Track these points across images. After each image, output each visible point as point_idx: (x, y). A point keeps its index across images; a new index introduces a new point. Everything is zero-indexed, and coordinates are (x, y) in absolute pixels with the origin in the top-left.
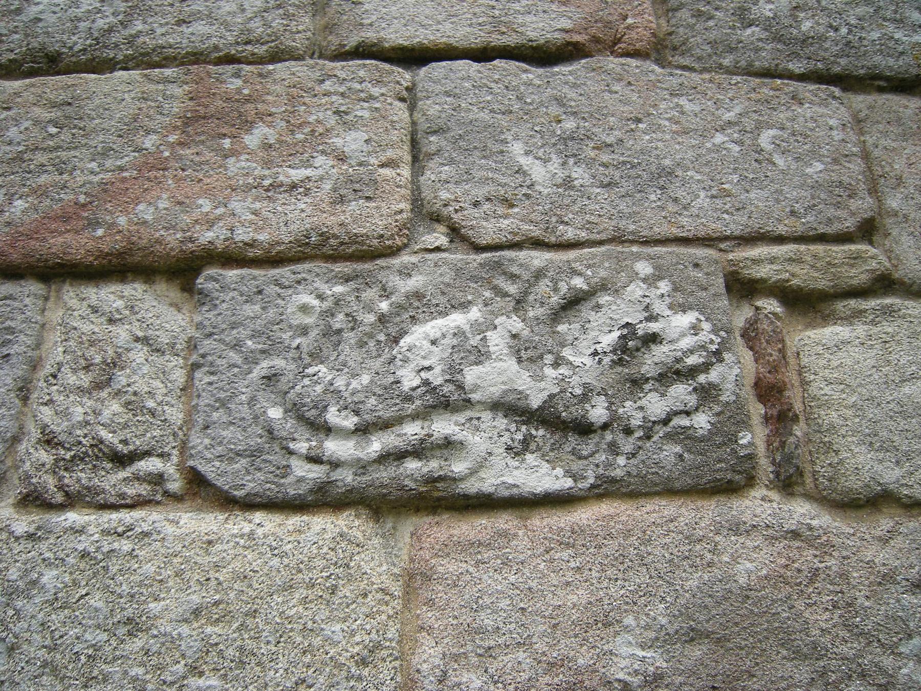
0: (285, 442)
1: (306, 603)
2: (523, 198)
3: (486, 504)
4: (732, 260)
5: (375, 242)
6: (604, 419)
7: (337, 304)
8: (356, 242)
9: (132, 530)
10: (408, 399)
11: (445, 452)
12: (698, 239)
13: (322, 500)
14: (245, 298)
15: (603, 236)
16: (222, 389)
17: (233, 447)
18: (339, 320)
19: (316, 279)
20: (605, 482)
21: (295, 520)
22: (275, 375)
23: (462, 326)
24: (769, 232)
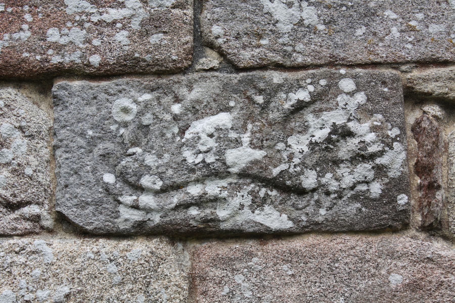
0: (116, 197)
1: (132, 292)
2: (270, 33)
3: (237, 235)
4: (409, 79)
5: (170, 65)
6: (313, 186)
7: (146, 107)
8: (158, 65)
9: (24, 249)
10: (192, 171)
11: (214, 204)
12: (388, 63)
13: (140, 231)
14: (85, 102)
15: (322, 62)
16: (75, 162)
17: (84, 199)
18: (147, 119)
19: (131, 90)
20: (312, 224)
21: (124, 244)
22: (108, 154)
23: (226, 124)
24: (438, 58)
